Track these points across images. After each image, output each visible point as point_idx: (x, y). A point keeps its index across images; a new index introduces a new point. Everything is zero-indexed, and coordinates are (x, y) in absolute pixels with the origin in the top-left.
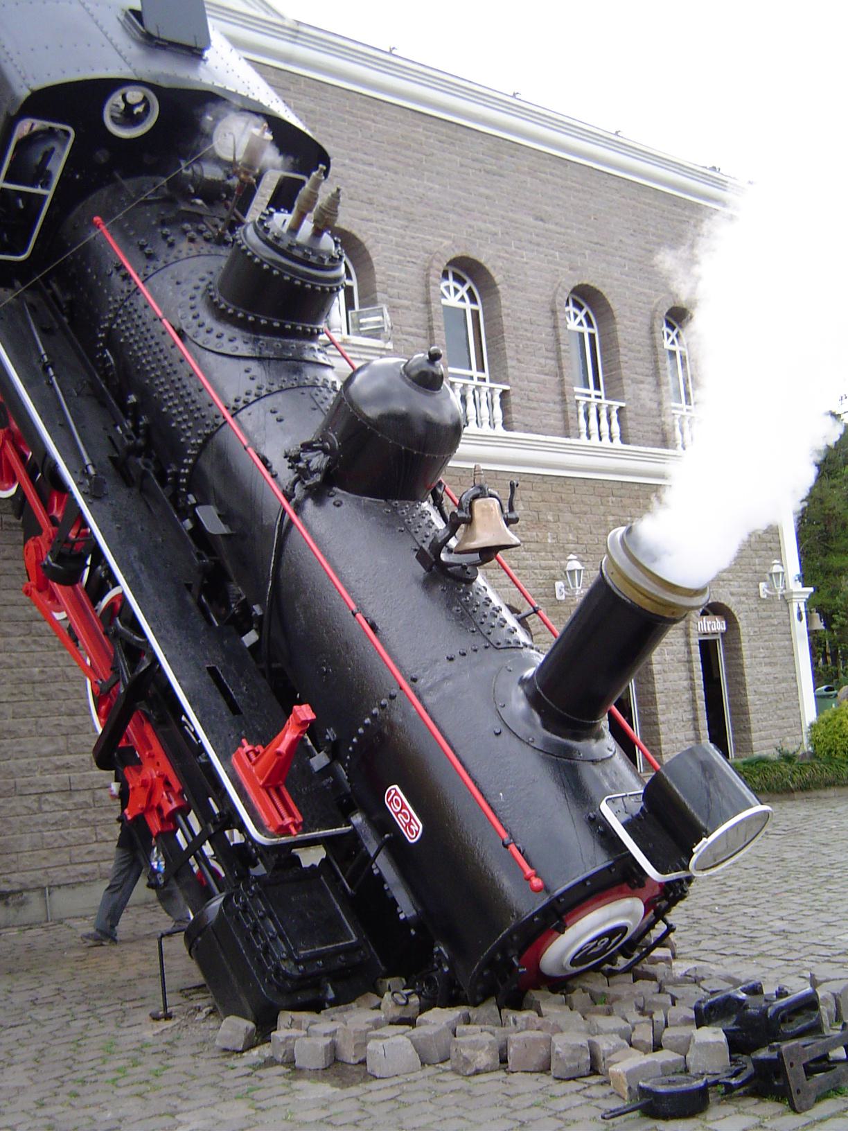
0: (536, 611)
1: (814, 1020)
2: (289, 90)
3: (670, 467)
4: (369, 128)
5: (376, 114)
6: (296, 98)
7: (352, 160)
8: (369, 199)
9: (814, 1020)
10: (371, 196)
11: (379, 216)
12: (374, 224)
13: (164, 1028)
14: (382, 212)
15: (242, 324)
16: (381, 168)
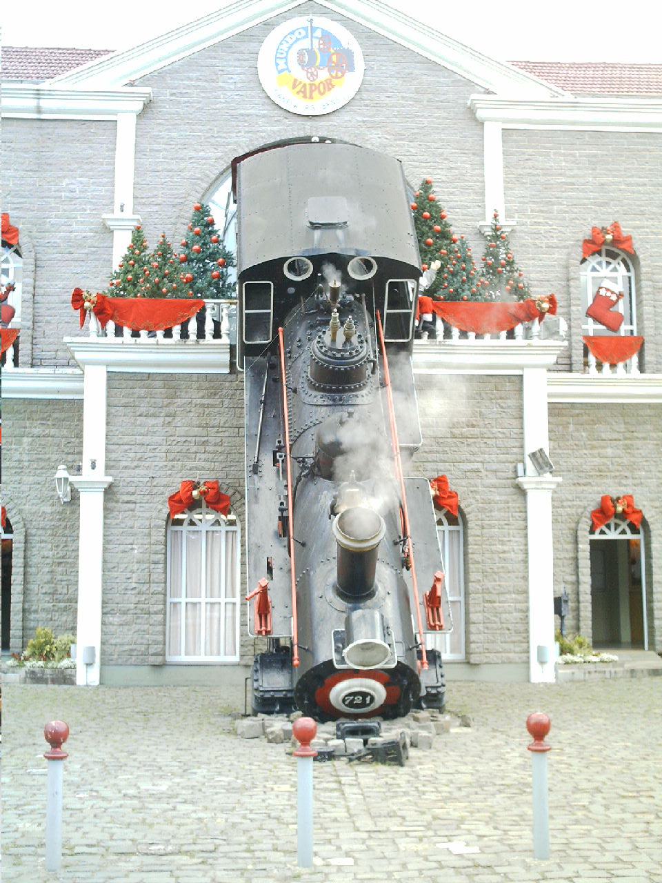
0: (57, 351)
1: (239, 369)
2: (575, 144)
3: (84, 397)
4: (644, 157)
5: (651, 144)
6: (581, 149)
7: (627, 185)
8: (641, 211)
9: (239, 369)
10: (642, 208)
11: (650, 223)
12: (645, 230)
13: (516, 655)
14: (652, 219)
15: (324, 390)
16: (653, 185)
